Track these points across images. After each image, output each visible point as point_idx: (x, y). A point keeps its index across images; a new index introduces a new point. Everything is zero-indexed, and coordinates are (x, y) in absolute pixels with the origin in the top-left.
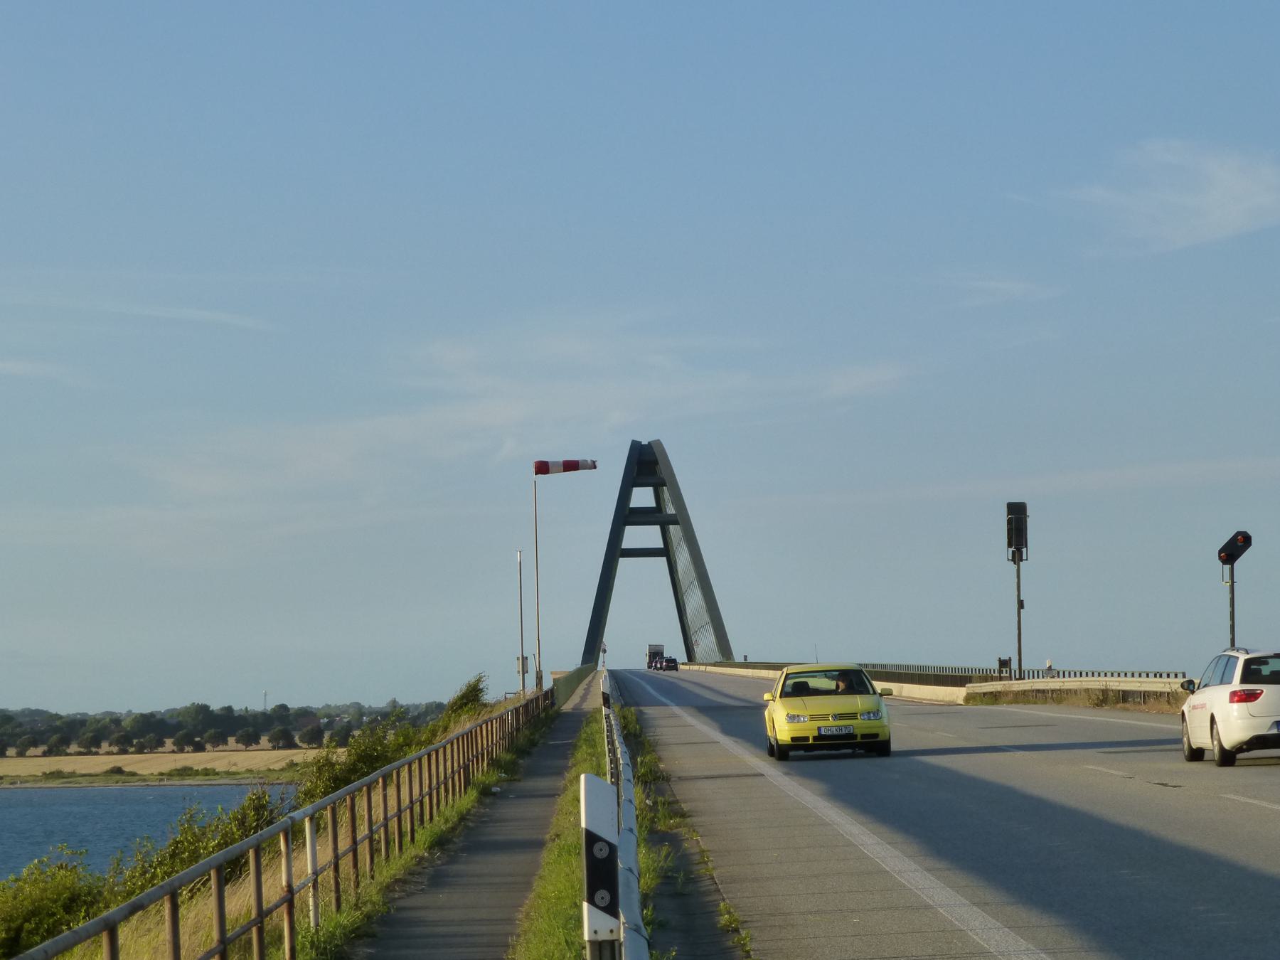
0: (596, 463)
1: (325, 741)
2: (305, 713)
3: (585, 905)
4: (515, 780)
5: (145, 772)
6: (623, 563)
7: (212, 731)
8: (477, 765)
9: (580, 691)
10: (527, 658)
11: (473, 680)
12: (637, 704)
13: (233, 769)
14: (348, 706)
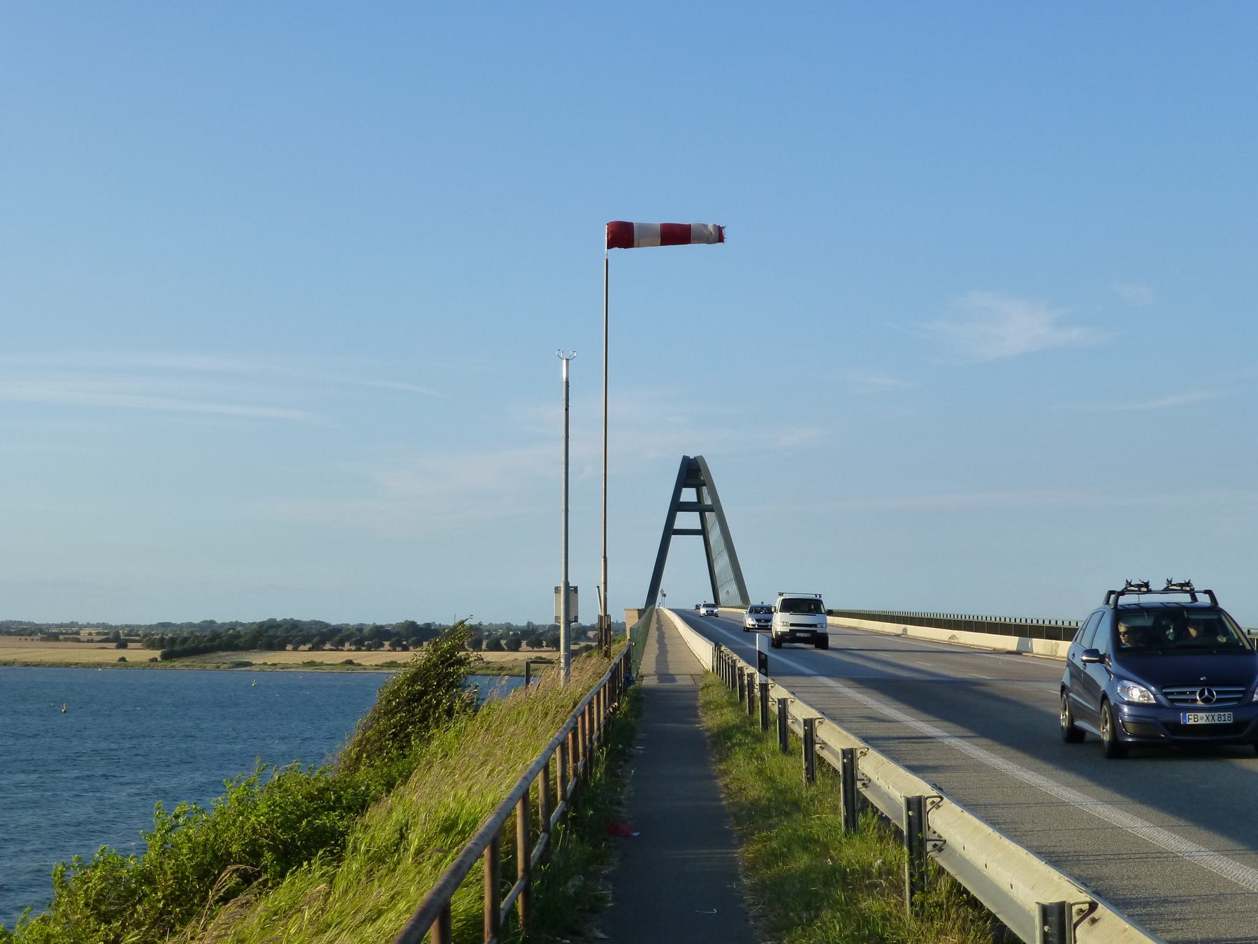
2: (491, 629)
5: (368, 664)
6: (674, 539)
7: (414, 638)
10: (576, 589)
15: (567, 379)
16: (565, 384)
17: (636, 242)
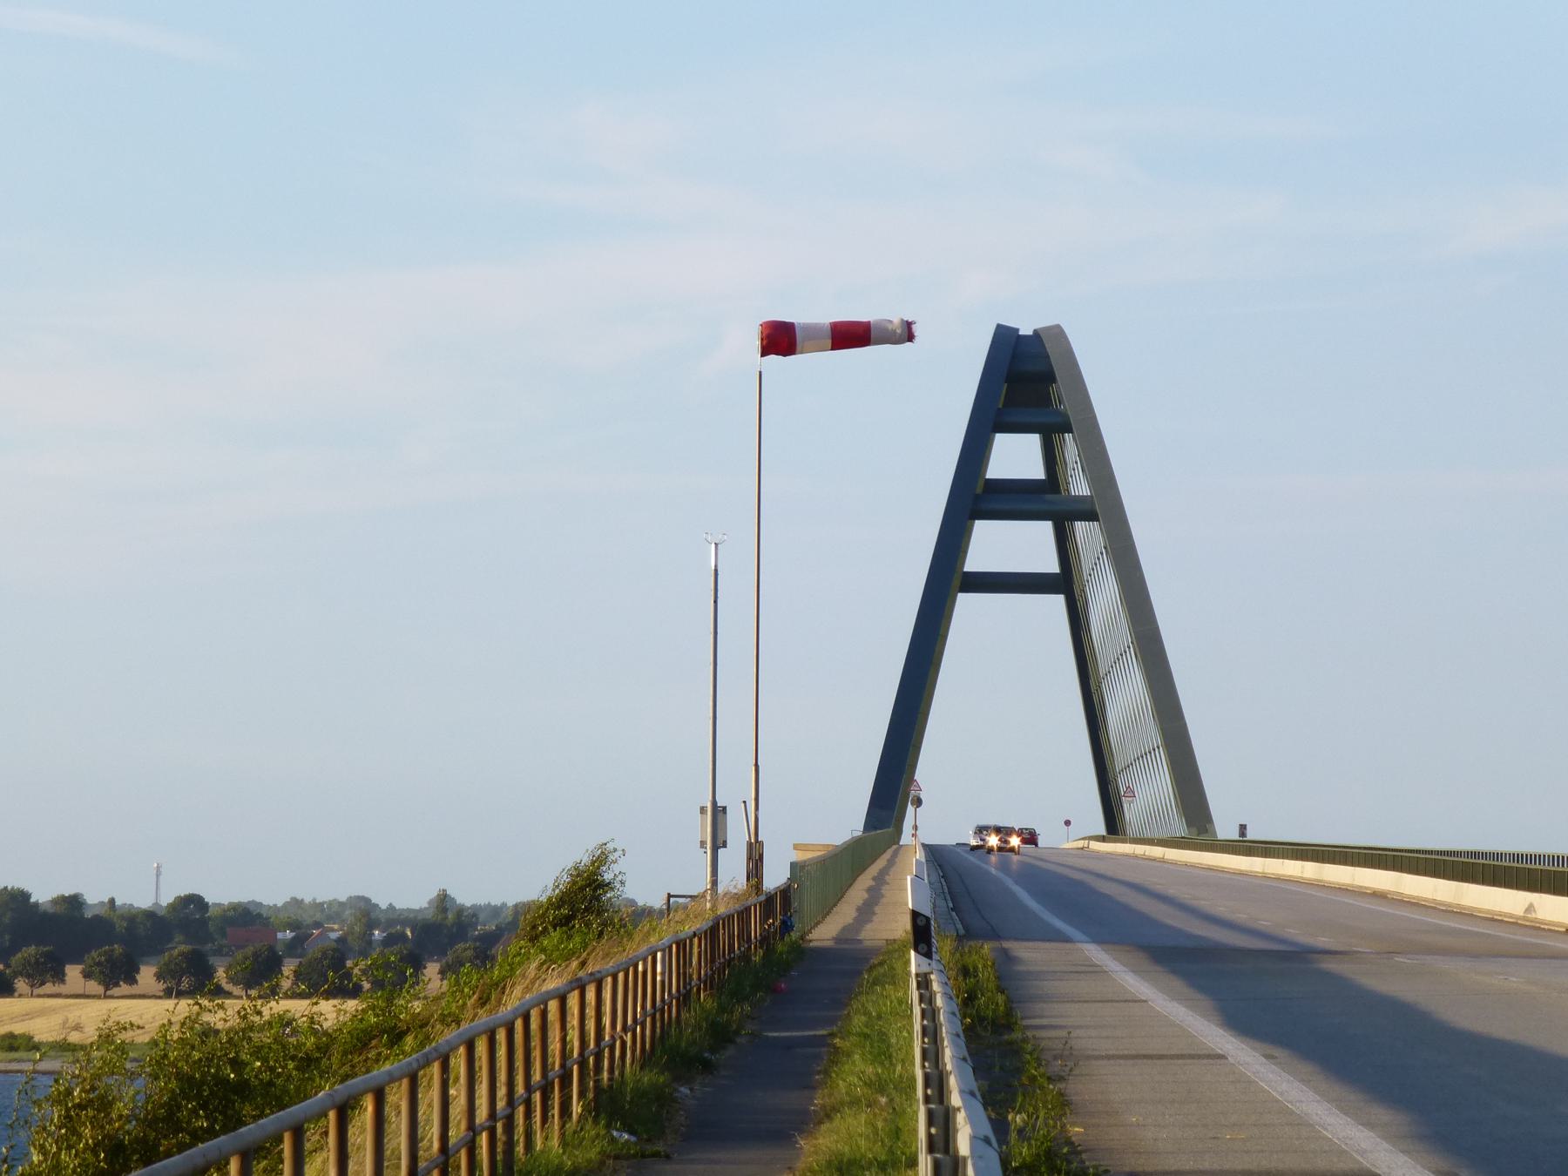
0: (914, 327)
1: (286, 984)
2: (245, 918)
3: (912, 953)
4: (656, 1155)
6: (967, 605)
8: (562, 1089)
9: (857, 894)
10: (724, 809)
11: (586, 860)
12: (995, 935)
13: (74, 1038)
14: (341, 904)
15: (716, 566)
16: (713, 572)
17: (799, 347)
